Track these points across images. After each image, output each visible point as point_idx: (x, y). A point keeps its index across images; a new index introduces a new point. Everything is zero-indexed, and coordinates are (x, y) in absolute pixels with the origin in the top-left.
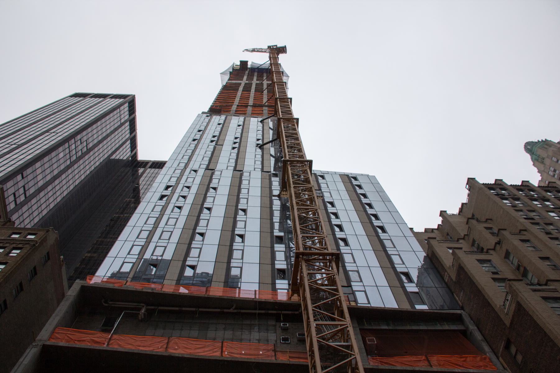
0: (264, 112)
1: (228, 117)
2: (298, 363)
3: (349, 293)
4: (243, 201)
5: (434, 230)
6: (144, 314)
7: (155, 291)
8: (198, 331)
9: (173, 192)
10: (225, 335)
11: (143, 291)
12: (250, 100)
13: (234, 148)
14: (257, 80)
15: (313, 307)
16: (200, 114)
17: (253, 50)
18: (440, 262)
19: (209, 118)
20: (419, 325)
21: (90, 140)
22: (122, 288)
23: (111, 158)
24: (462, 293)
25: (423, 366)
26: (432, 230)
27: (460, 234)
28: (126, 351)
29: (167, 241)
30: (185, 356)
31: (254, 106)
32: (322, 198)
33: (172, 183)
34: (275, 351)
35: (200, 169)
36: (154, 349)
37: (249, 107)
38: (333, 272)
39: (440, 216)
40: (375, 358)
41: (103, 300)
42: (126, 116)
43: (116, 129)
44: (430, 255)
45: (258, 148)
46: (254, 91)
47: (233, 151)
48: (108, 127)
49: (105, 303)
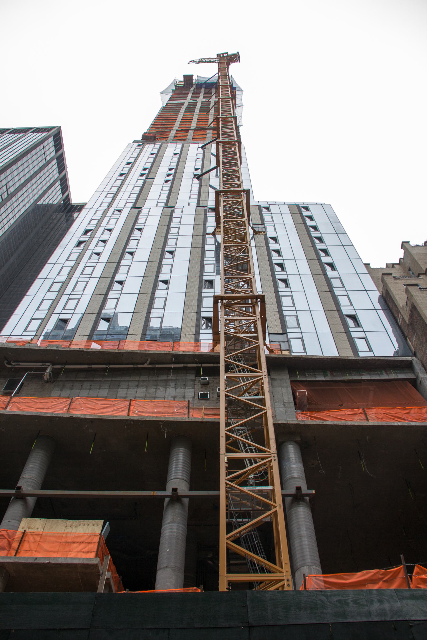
0: (208, 136)
1: (163, 144)
2: (213, 421)
3: (283, 341)
5: (395, 266)
6: (50, 374)
7: (60, 349)
8: (108, 390)
9: (92, 238)
10: (137, 393)
11: (47, 349)
12: (193, 122)
13: (167, 181)
14: (204, 98)
15: (225, 358)
16: (130, 144)
17: (201, 61)
18: (394, 302)
19: (141, 147)
20: (361, 375)
21: (11, 183)
22: (24, 348)
23: (38, 203)
24: (415, 337)
25: (358, 420)
26: (393, 265)
27: (422, 268)
28: (24, 414)
30: (88, 417)
31: (197, 129)
32: (264, 234)
33: (92, 227)
34: (188, 408)
35: (125, 208)
36: (55, 411)
37: (190, 131)
38: (255, 318)
39: (402, 248)
40: (305, 412)
41: (5, 362)
42: (51, 153)
43: (41, 169)
44: (384, 295)
45: (196, 179)
46: (198, 111)
47: (166, 185)
48: (31, 167)
49: (7, 363)
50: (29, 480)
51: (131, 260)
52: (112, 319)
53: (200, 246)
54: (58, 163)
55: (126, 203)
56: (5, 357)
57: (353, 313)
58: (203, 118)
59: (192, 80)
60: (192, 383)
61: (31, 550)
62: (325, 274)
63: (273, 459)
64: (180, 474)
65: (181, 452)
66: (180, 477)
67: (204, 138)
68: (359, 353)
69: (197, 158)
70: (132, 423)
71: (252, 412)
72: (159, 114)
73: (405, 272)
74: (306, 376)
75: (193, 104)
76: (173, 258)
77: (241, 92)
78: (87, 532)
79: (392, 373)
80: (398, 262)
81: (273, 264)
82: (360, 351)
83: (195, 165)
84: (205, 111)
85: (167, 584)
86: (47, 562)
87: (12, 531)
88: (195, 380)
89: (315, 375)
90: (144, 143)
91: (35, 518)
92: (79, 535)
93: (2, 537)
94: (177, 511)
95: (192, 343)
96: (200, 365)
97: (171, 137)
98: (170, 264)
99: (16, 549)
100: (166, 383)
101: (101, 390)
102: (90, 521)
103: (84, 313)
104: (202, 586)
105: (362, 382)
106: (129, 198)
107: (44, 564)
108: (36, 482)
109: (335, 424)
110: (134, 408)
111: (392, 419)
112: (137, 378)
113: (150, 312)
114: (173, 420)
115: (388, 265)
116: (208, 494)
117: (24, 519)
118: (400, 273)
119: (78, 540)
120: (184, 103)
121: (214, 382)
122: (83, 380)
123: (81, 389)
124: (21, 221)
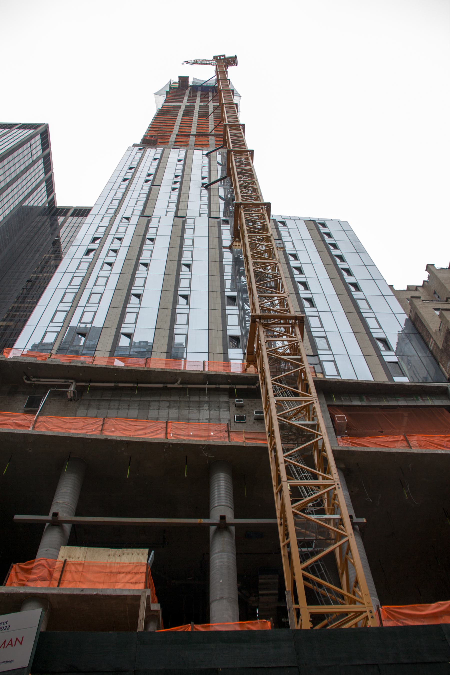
0: (210, 142)
1: (166, 149)
4: (186, 255)
5: (419, 288)
6: (74, 392)
7: (85, 365)
8: (137, 411)
9: (101, 246)
11: (71, 364)
12: (193, 128)
13: (174, 189)
14: (201, 102)
16: (131, 147)
17: (195, 62)
18: (425, 326)
19: (142, 151)
20: (397, 401)
22: (46, 363)
23: (23, 205)
25: (401, 447)
26: (417, 288)
28: (55, 434)
29: (97, 305)
30: (124, 439)
31: (198, 135)
32: (282, 250)
33: (100, 234)
34: (228, 431)
36: (87, 432)
37: (191, 137)
39: (426, 270)
40: (345, 438)
41: (24, 378)
42: (38, 151)
43: (27, 169)
44: (413, 318)
45: (204, 188)
46: (197, 116)
47: (173, 193)
48: (17, 165)
49: (26, 379)
50: (64, 505)
51: (110, 272)
52: (89, 334)
53: (178, 246)
54: (45, 163)
55: (108, 209)
56: (24, 372)
57: (382, 336)
58: (203, 124)
59: (188, 82)
60: (226, 405)
61: (74, 581)
62: (350, 295)
63: (337, 487)
64: (224, 501)
65: (222, 477)
66: (224, 504)
67: (207, 145)
68: (311, 328)
69: (203, 166)
70: (171, 446)
71: (303, 437)
72: (156, 116)
73: (429, 295)
74: (342, 401)
75: (191, 108)
76: (148, 270)
77: (239, 97)
78: (132, 561)
79: (428, 399)
80: (421, 285)
81: (295, 283)
82: (327, 375)
83: (175, 172)
84: (204, 116)
85: (224, 616)
86: (95, 593)
87: (52, 560)
88: (229, 402)
89: (351, 399)
90: (145, 146)
91: (75, 547)
92: (125, 565)
93: (41, 567)
94: (226, 539)
95: (221, 363)
96: (234, 386)
97: (172, 141)
98: (189, 278)
99: (58, 580)
100: (199, 405)
101: (130, 410)
102: (134, 550)
103: (102, 326)
104: (271, 618)
105: (399, 408)
106: (111, 204)
107: (91, 596)
108: (71, 508)
109: (379, 451)
110: (171, 430)
111: (435, 447)
112: (168, 399)
113: (121, 328)
114: (214, 444)
115: (409, 287)
116: (257, 522)
117: (63, 548)
118: (425, 296)
119: (123, 570)
120: (181, 106)
121: (248, 404)
122: (110, 399)
123: (109, 409)
124: (5, 223)
